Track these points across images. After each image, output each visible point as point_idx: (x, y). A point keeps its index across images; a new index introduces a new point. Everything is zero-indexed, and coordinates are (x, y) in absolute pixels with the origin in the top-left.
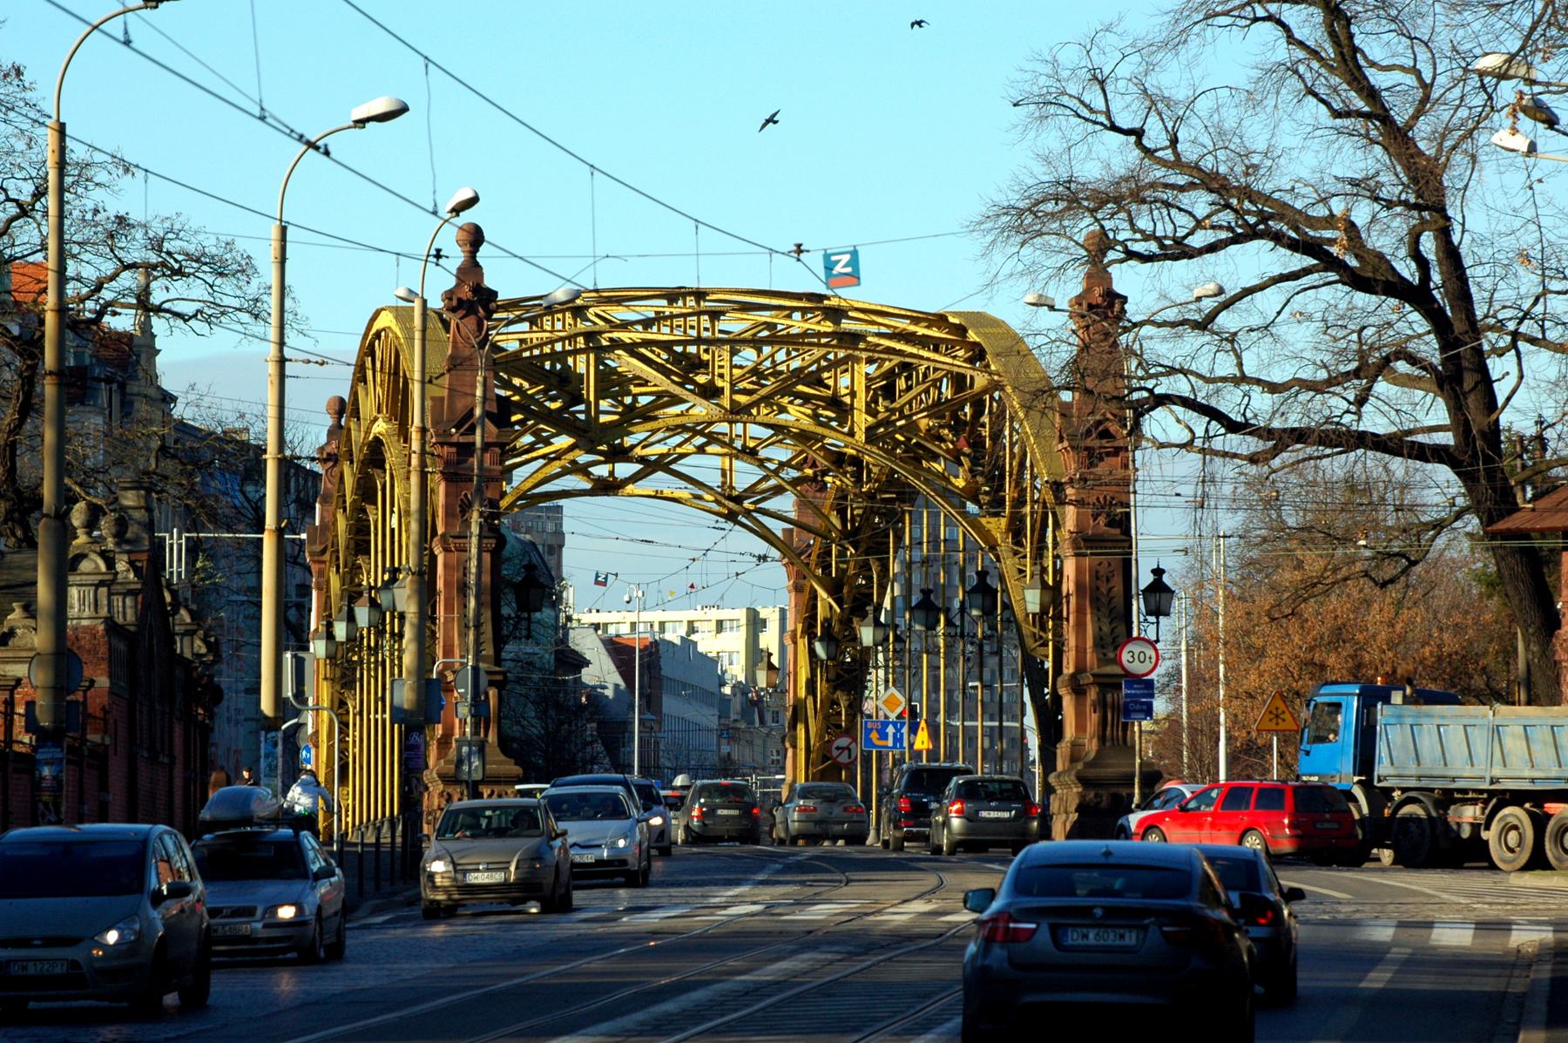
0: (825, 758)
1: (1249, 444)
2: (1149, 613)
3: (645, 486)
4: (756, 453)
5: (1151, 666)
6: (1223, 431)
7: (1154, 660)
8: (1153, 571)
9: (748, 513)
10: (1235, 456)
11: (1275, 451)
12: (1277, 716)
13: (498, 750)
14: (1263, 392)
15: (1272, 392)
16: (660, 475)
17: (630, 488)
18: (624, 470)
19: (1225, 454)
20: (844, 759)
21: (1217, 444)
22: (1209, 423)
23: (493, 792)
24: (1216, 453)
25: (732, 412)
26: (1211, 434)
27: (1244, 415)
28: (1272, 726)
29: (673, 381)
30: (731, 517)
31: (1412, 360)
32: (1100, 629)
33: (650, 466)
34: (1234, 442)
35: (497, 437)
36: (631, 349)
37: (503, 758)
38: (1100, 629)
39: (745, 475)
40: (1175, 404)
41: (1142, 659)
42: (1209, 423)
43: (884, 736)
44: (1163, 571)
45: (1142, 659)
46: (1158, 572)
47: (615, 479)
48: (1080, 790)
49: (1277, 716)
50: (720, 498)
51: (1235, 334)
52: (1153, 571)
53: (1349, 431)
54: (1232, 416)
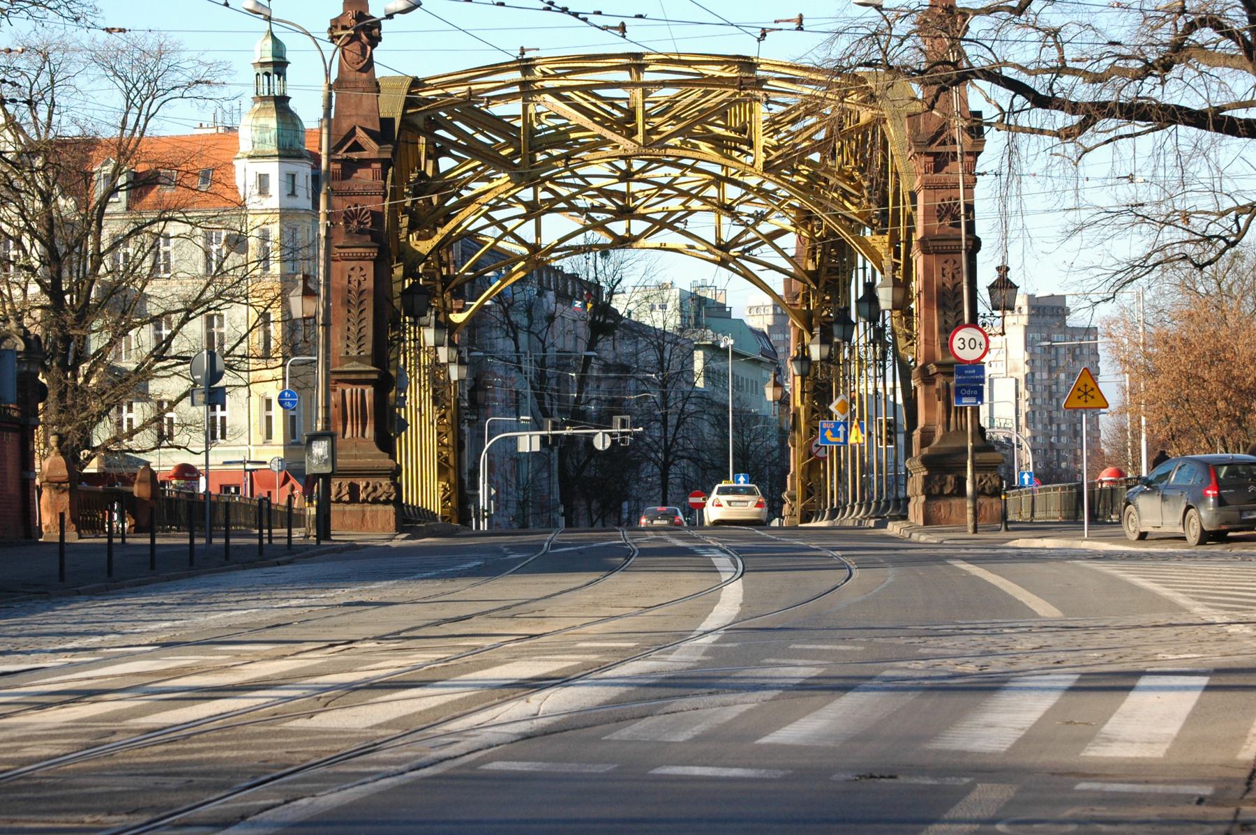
0: (810, 455)
1: (1061, 119)
2: (995, 308)
3: (655, 240)
4: (733, 209)
5: (981, 352)
6: (1028, 105)
7: (984, 346)
8: (998, 269)
9: (735, 261)
10: (1041, 132)
11: (1083, 126)
12: (1086, 393)
13: (374, 445)
14: (1084, 82)
15: (1094, 82)
16: (666, 231)
17: (642, 242)
18: (638, 227)
19: (1032, 131)
20: (821, 454)
21: (1023, 120)
22: (1014, 97)
23: (368, 484)
24: (1023, 130)
25: (645, 146)
26: (1016, 109)
27: (1051, 88)
28: (1081, 403)
29: (595, 122)
30: (723, 263)
31: (1218, 26)
32: (946, 322)
33: (661, 225)
34: (1038, 117)
35: (379, 152)
36: (556, 93)
37: (378, 451)
38: (946, 322)
39: (730, 230)
40: (978, 78)
41: (972, 346)
42: (1014, 97)
43: (836, 434)
44: (1008, 269)
45: (972, 346)
46: (1003, 270)
47: (630, 234)
48: (926, 473)
49: (1086, 393)
50: (710, 248)
51: (1059, 30)
52: (998, 269)
53: (1158, 103)
54: (1040, 92)
